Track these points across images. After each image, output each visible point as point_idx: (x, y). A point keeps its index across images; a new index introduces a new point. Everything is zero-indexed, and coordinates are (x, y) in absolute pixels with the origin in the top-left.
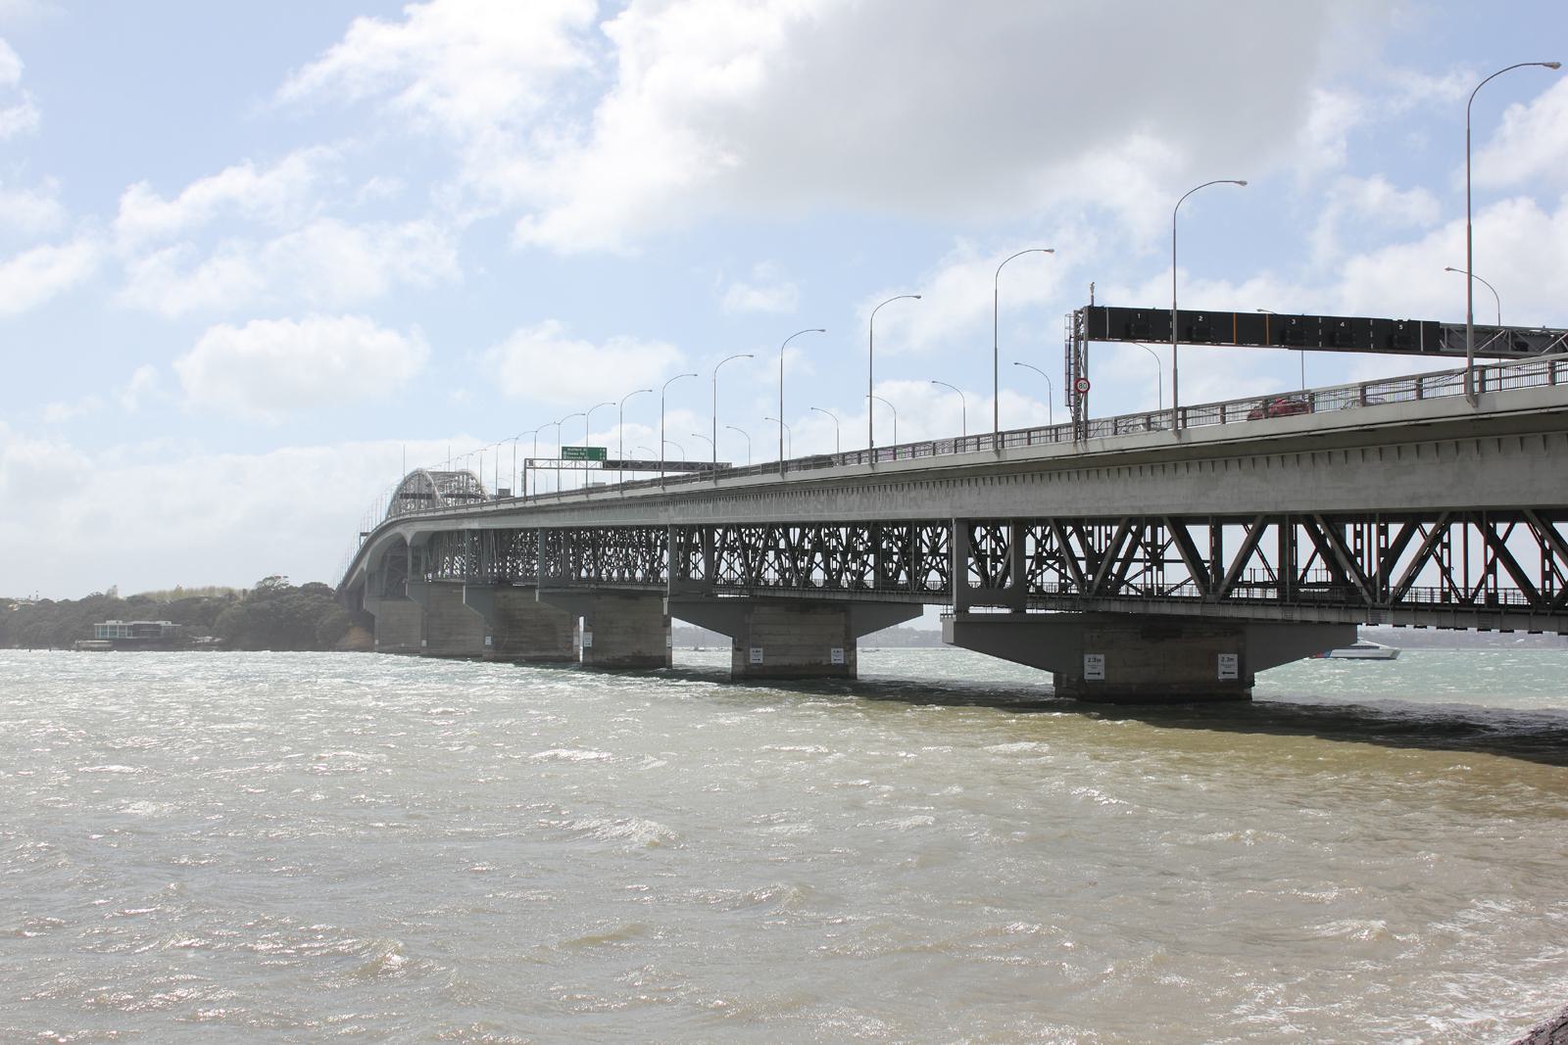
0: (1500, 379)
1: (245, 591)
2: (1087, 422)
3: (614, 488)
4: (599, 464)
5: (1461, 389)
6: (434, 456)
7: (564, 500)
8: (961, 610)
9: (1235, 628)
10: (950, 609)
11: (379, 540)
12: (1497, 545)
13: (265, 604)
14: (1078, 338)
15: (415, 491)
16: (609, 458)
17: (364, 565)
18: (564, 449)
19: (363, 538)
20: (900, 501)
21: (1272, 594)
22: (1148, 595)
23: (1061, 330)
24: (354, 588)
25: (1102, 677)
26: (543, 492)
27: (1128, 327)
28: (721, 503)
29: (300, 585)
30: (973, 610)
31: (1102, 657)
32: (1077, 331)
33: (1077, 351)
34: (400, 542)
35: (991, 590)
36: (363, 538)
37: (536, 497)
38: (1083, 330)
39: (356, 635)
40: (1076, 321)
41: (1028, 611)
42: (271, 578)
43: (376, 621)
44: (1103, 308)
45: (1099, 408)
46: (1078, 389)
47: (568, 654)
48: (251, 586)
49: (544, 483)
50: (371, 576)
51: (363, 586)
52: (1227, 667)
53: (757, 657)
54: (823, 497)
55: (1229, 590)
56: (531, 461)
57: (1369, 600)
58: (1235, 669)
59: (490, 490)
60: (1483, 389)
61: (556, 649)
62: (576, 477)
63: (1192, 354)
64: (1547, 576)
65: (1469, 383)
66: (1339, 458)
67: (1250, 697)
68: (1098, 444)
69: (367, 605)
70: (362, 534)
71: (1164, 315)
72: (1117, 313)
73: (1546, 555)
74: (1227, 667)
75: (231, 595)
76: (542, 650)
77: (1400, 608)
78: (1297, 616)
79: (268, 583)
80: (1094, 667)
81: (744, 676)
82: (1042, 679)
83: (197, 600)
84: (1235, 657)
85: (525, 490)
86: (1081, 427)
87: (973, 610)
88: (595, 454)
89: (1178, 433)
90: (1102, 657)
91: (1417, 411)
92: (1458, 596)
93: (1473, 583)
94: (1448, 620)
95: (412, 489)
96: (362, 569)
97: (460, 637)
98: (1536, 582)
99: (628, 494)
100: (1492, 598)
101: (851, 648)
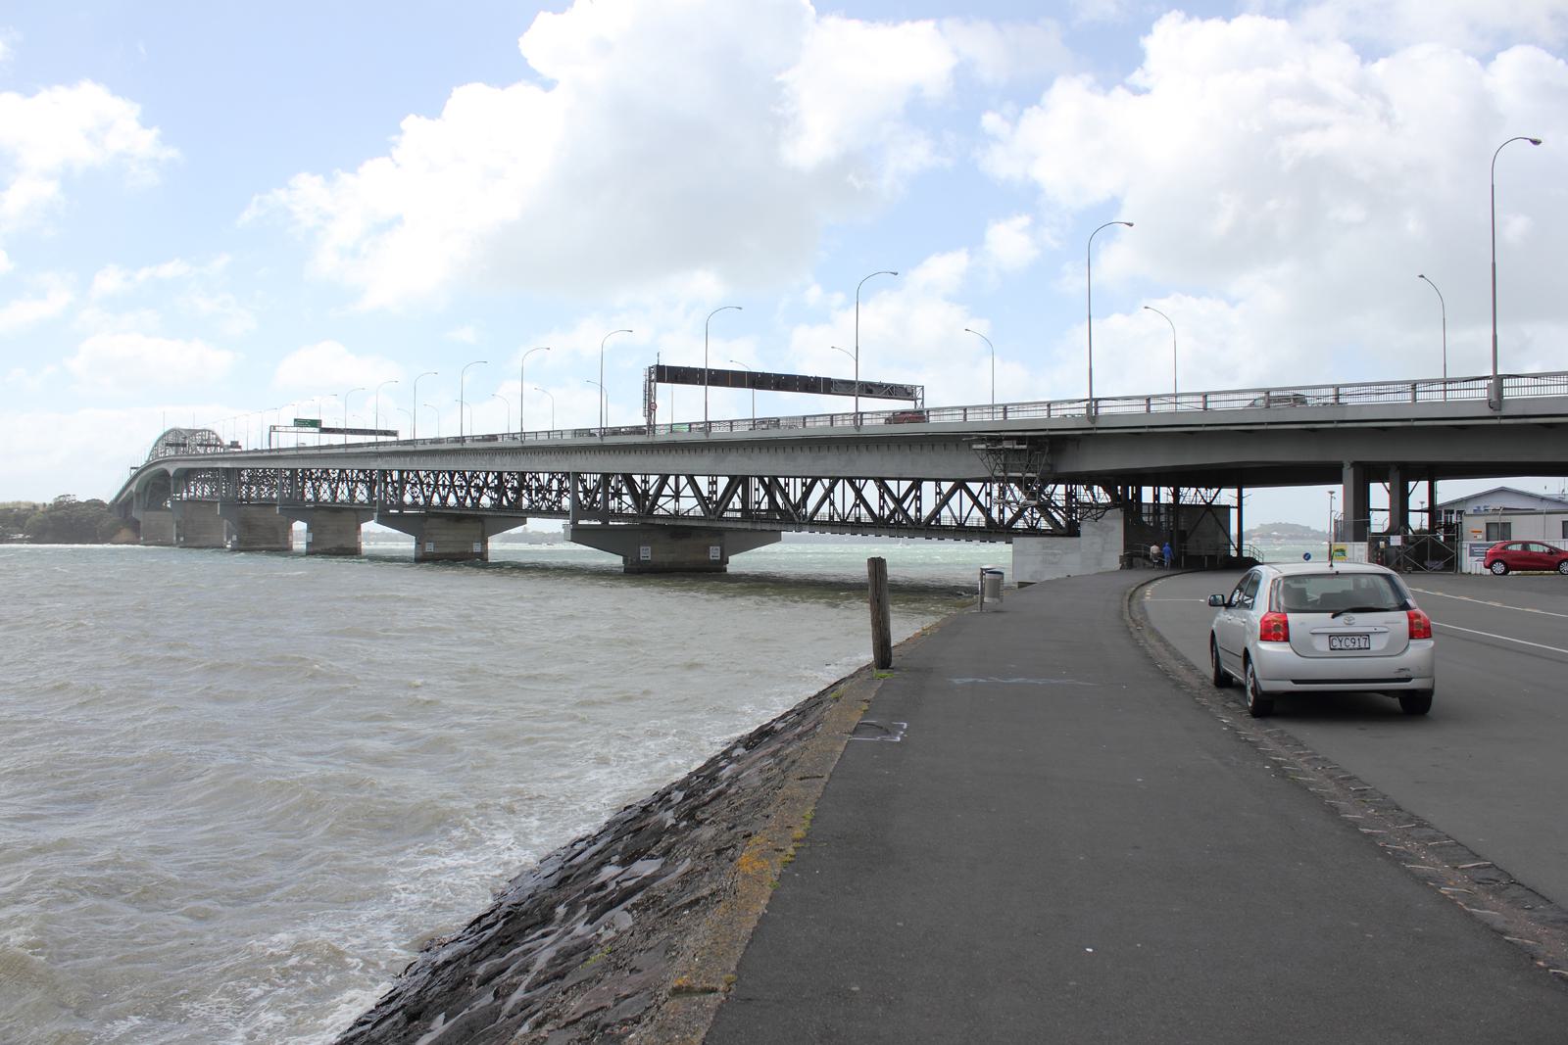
0: (1445, 390)
1: (45, 505)
2: (655, 425)
3: (339, 446)
4: (317, 430)
5: (1084, 411)
6: (185, 419)
7: (350, 450)
8: (575, 522)
9: (718, 533)
10: (568, 522)
11: (145, 473)
12: (858, 492)
13: (59, 513)
14: (650, 381)
15: (176, 440)
16: (323, 426)
17: (133, 488)
18: (295, 420)
19: (133, 471)
20: (537, 461)
21: (739, 515)
22: (670, 517)
23: (641, 379)
24: (123, 504)
25: (649, 558)
26: (324, 444)
27: (676, 376)
28: (415, 458)
29: (84, 501)
30: (581, 522)
31: (649, 548)
32: (650, 377)
33: (650, 390)
34: (165, 473)
35: (590, 512)
36: (133, 471)
37: (280, 450)
38: (653, 377)
39: (126, 533)
40: (650, 372)
41: (611, 523)
42: (64, 496)
43: (142, 525)
44: (664, 366)
45: (662, 418)
46: (650, 408)
47: (286, 546)
48: (49, 500)
49: (288, 440)
50: (138, 494)
51: (132, 499)
52: (714, 553)
53: (430, 548)
54: (487, 457)
55: (723, 513)
56: (274, 427)
57: (797, 520)
58: (719, 555)
59: (227, 442)
60: (861, 424)
61: (277, 543)
62: (311, 439)
63: (717, 392)
64: (881, 508)
65: (855, 420)
66: (789, 450)
67: (725, 570)
68: (662, 435)
69: (136, 514)
70: (132, 468)
71: (702, 371)
72: (671, 369)
73: (882, 497)
74: (714, 553)
75: (35, 507)
76: (269, 543)
77: (811, 523)
78: (759, 527)
79: (61, 499)
80: (646, 553)
81: (422, 559)
82: (617, 561)
83: (11, 510)
84: (719, 548)
85: (270, 444)
86: (652, 427)
87: (581, 522)
88: (315, 423)
89: (522, 442)
90: (649, 548)
91: (830, 432)
92: (839, 516)
93: (847, 511)
94: (837, 529)
95: (171, 439)
96: (131, 491)
97: (205, 536)
98: (876, 512)
99: (350, 450)
100: (858, 519)
101: (485, 542)
